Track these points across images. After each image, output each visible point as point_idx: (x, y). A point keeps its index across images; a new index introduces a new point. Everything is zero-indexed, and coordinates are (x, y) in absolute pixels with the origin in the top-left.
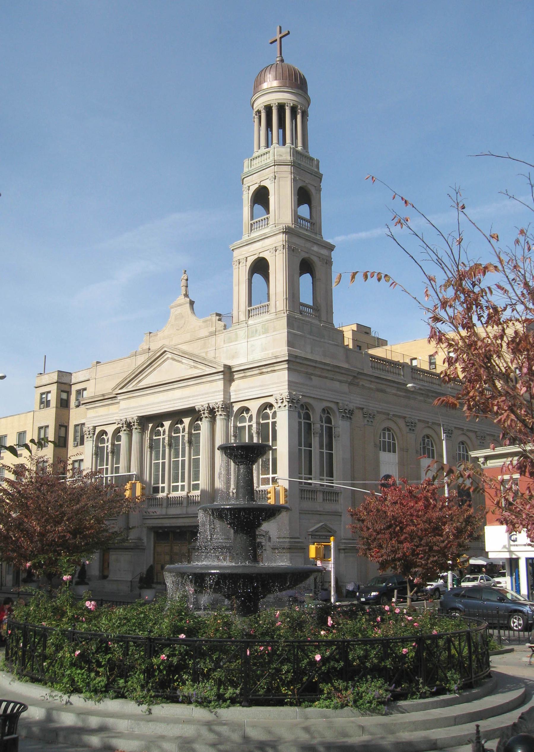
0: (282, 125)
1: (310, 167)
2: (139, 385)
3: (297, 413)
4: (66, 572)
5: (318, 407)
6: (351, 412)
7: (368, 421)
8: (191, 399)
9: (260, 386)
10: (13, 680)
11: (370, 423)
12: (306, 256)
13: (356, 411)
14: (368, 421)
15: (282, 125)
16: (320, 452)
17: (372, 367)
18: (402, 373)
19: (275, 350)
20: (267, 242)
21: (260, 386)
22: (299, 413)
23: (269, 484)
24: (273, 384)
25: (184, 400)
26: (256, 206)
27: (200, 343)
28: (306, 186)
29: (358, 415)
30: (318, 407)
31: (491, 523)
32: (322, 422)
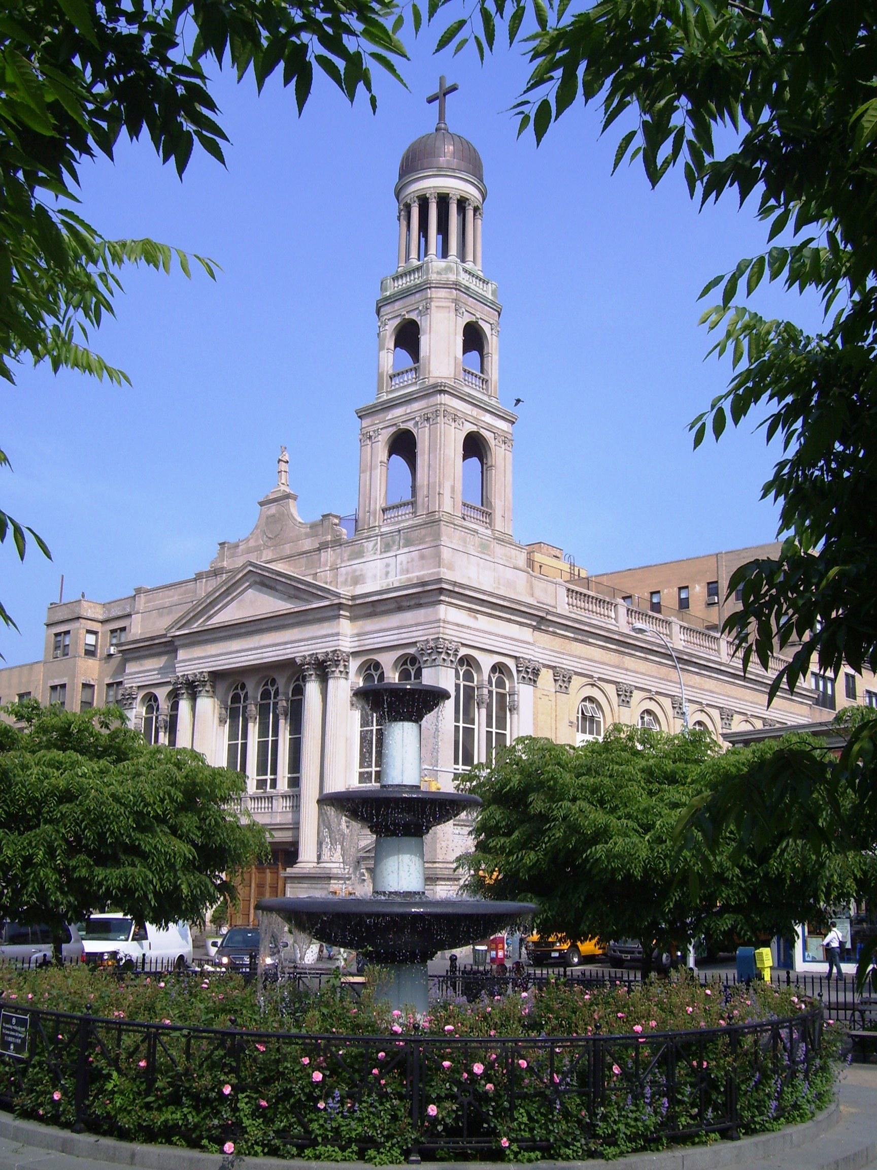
0: (443, 229)
1: (484, 293)
2: (209, 623)
3: (454, 671)
4: (438, 1101)
5: (486, 662)
6: (536, 672)
7: (561, 686)
8: (289, 646)
9: (398, 628)
10: (362, 828)
11: (563, 689)
12: (474, 429)
13: (544, 671)
14: (561, 686)
15: (443, 229)
16: (487, 732)
17: (568, 604)
18: (613, 616)
19: (422, 573)
20: (416, 406)
21: (398, 628)
22: (457, 672)
23: (473, 729)
24: (417, 625)
25: (277, 648)
26: (398, 349)
27: (303, 560)
28: (477, 322)
29: (546, 676)
30: (486, 662)
31: (190, 952)
32: (491, 686)
